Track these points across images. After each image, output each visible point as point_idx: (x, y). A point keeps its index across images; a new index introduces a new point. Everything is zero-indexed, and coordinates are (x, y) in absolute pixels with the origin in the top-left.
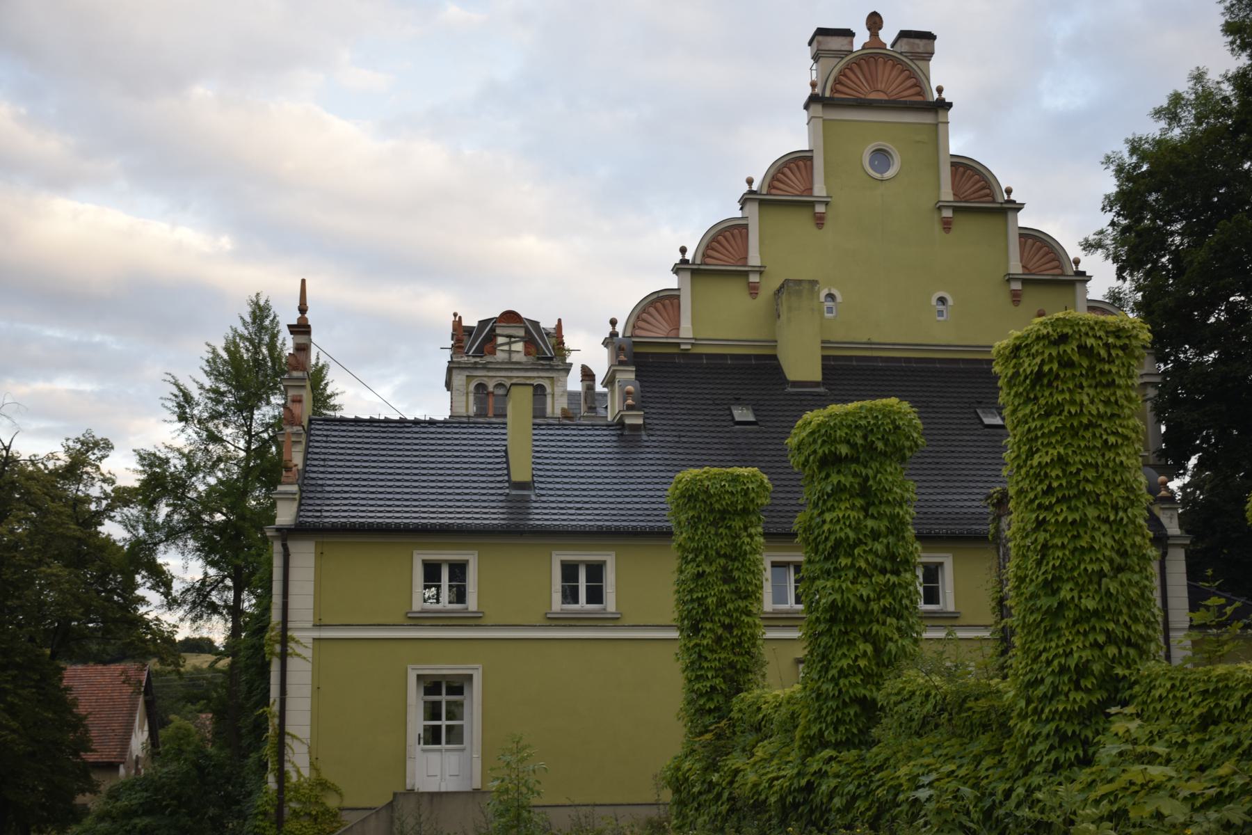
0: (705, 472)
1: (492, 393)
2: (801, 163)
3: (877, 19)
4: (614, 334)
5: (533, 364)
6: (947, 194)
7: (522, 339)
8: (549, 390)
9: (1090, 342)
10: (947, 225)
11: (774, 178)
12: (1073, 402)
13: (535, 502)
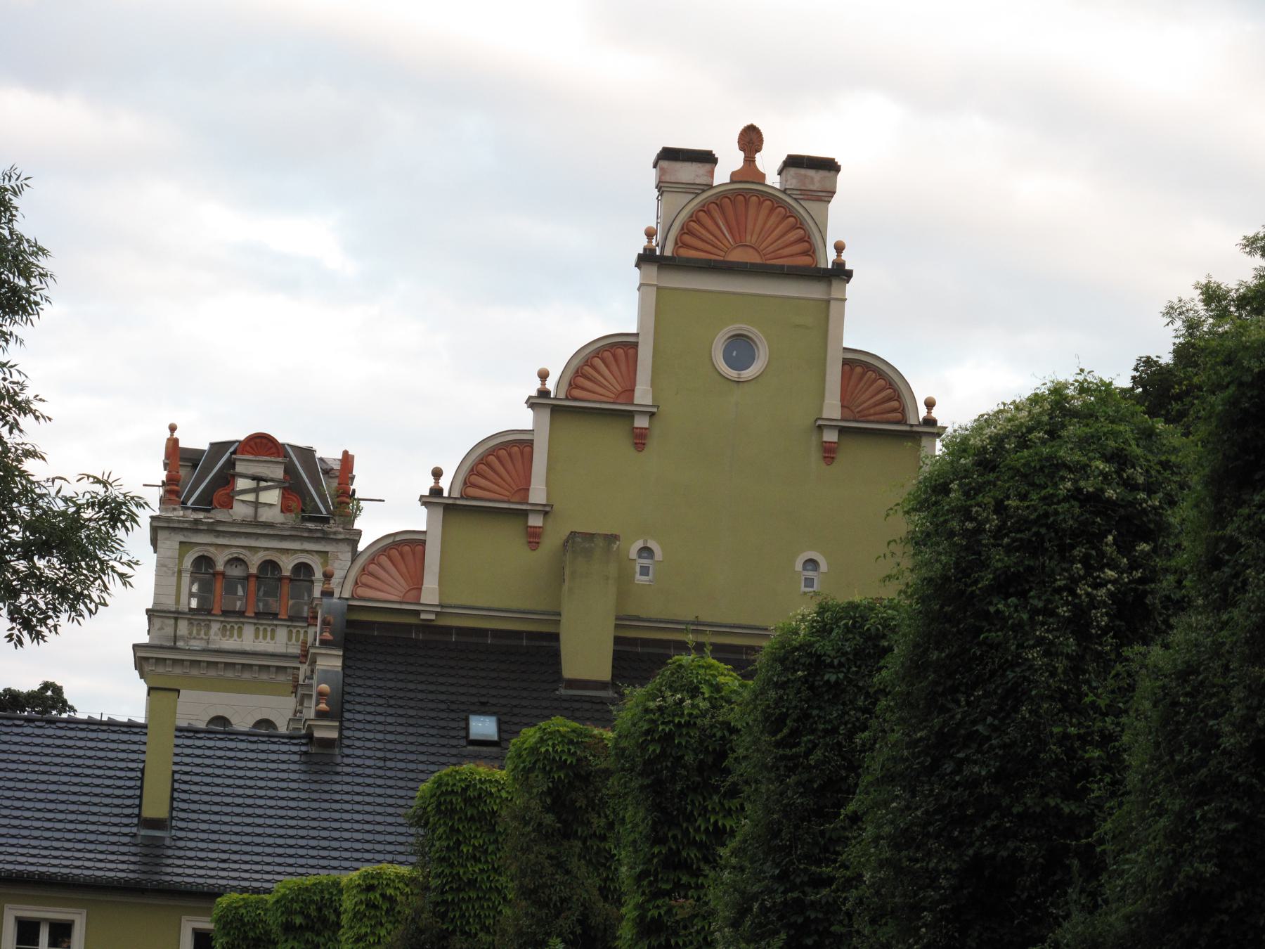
0: (243, 899)
1: (223, 574)
2: (620, 351)
3: (754, 136)
4: (436, 492)
5: (293, 528)
6: (832, 409)
7: (279, 484)
9: (389, 892)
10: (829, 453)
11: (579, 373)
12: (373, 934)
13: (169, 847)
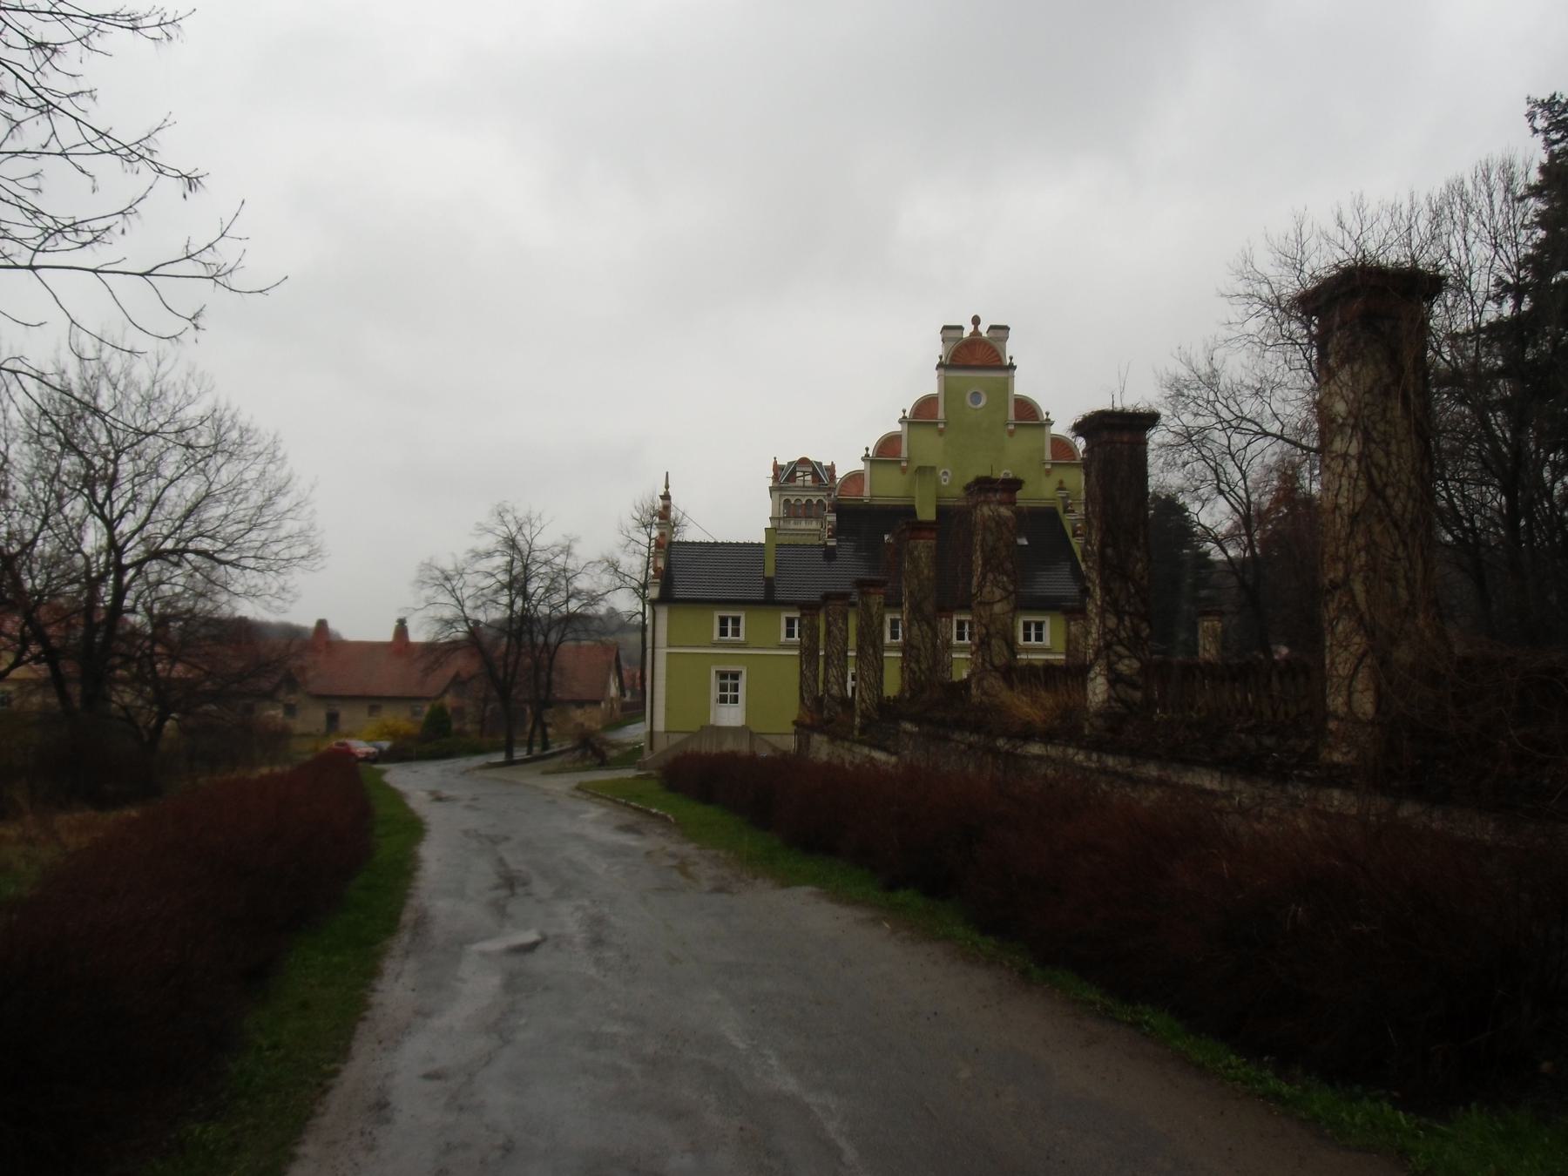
4: (867, 455)
10: (1011, 433)
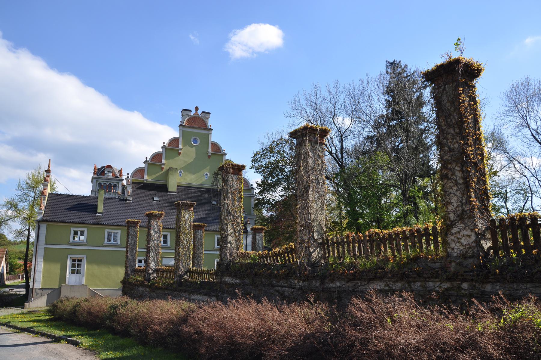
8: (117, 186)
10: (209, 157)
